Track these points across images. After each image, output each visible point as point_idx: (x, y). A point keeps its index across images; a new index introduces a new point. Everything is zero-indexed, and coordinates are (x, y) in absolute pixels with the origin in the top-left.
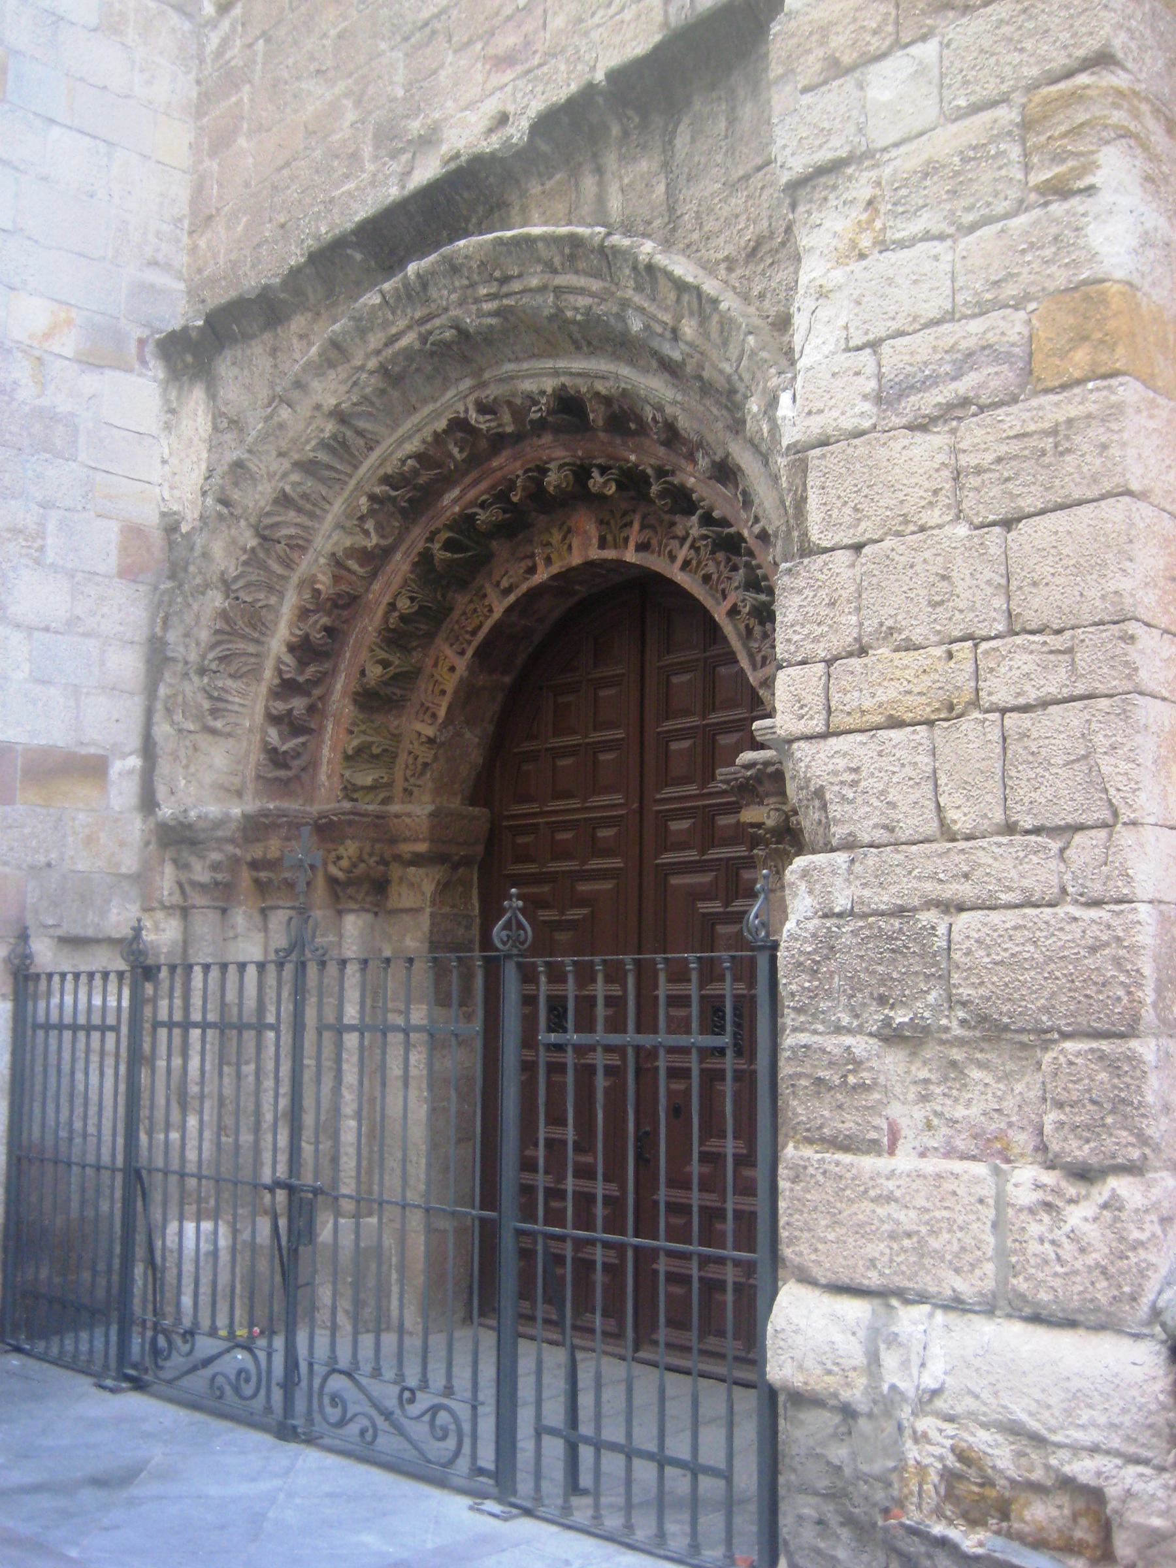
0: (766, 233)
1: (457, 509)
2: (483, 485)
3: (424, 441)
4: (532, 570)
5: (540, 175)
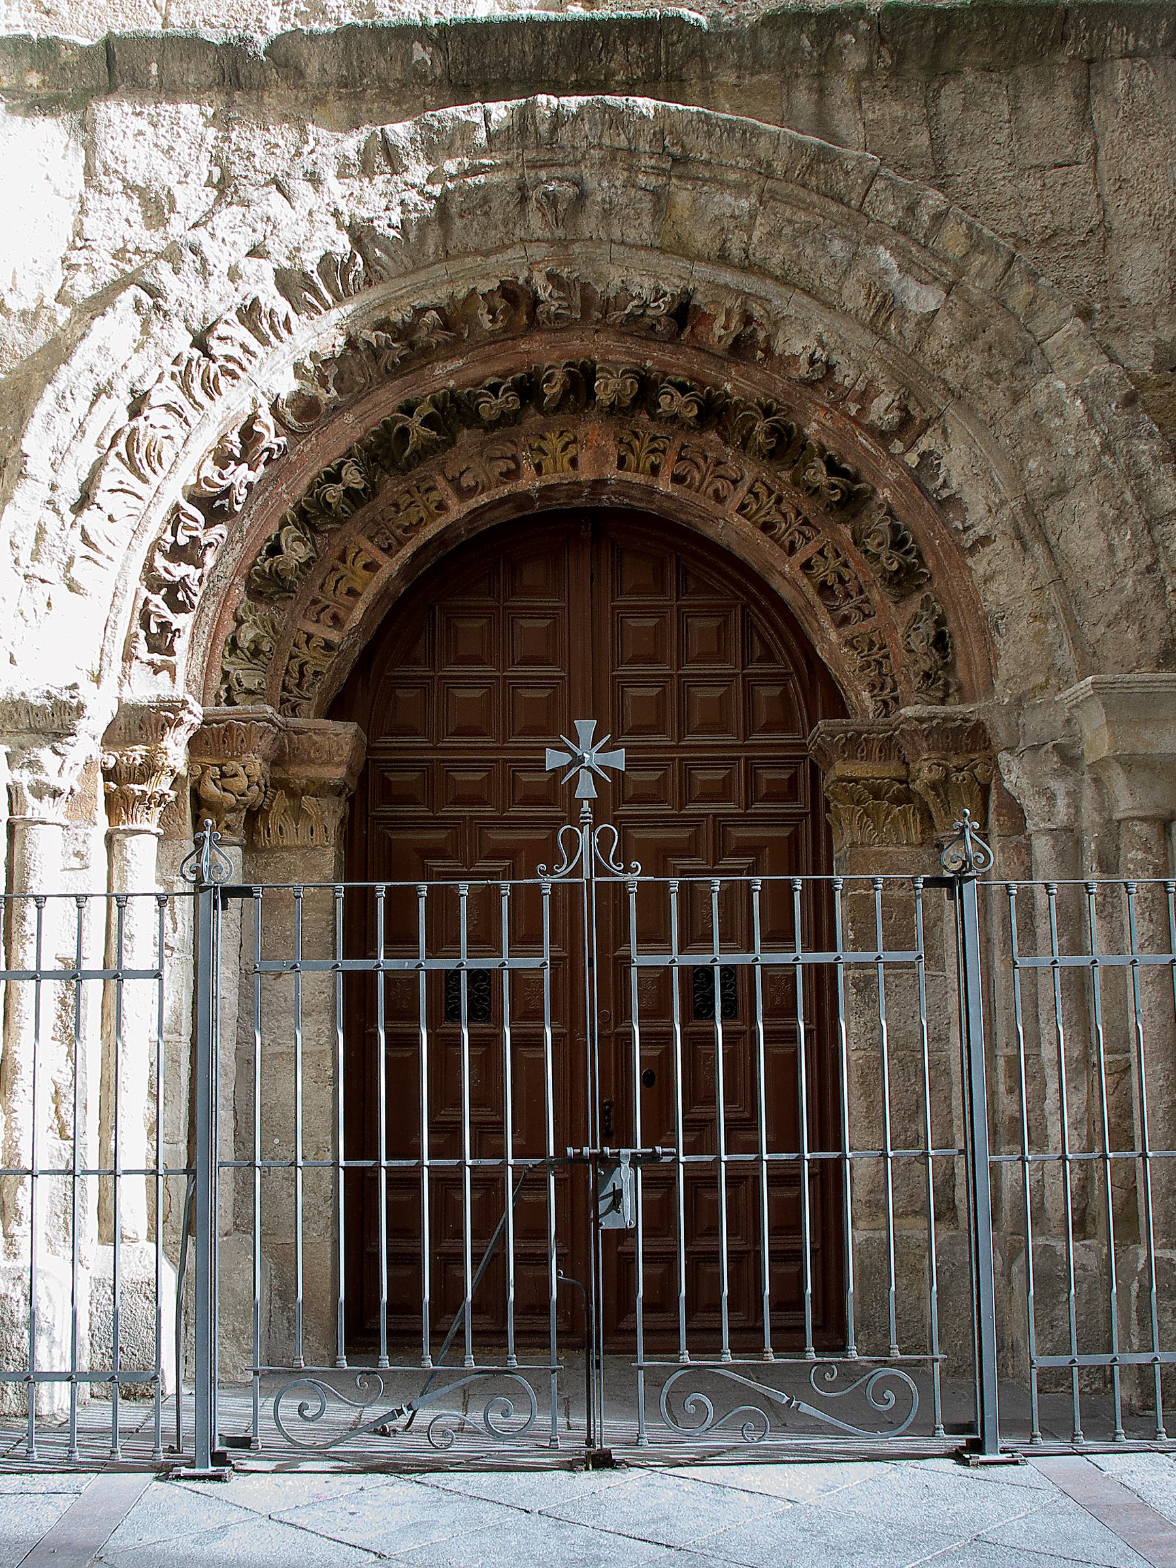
0: (1067, 227)
1: (452, 383)
2: (498, 367)
3: (452, 297)
4: (512, 475)
5: (739, 67)
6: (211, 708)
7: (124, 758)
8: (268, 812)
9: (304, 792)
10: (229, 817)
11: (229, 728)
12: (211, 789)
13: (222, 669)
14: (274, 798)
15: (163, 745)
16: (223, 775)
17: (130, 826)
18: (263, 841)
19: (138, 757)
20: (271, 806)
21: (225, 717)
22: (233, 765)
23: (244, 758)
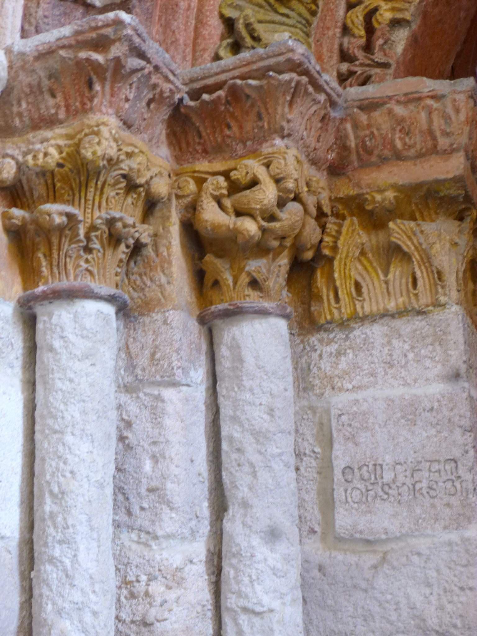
6: (207, 66)
7: (30, 157)
8: (331, 260)
9: (393, 212)
10: (256, 266)
11: (235, 94)
12: (212, 215)
13: (222, 16)
14: (339, 232)
15: (93, 119)
16: (235, 188)
17: (64, 284)
18: (327, 310)
19: (53, 151)
20: (335, 248)
21: (223, 77)
22: (254, 167)
23: (266, 149)
